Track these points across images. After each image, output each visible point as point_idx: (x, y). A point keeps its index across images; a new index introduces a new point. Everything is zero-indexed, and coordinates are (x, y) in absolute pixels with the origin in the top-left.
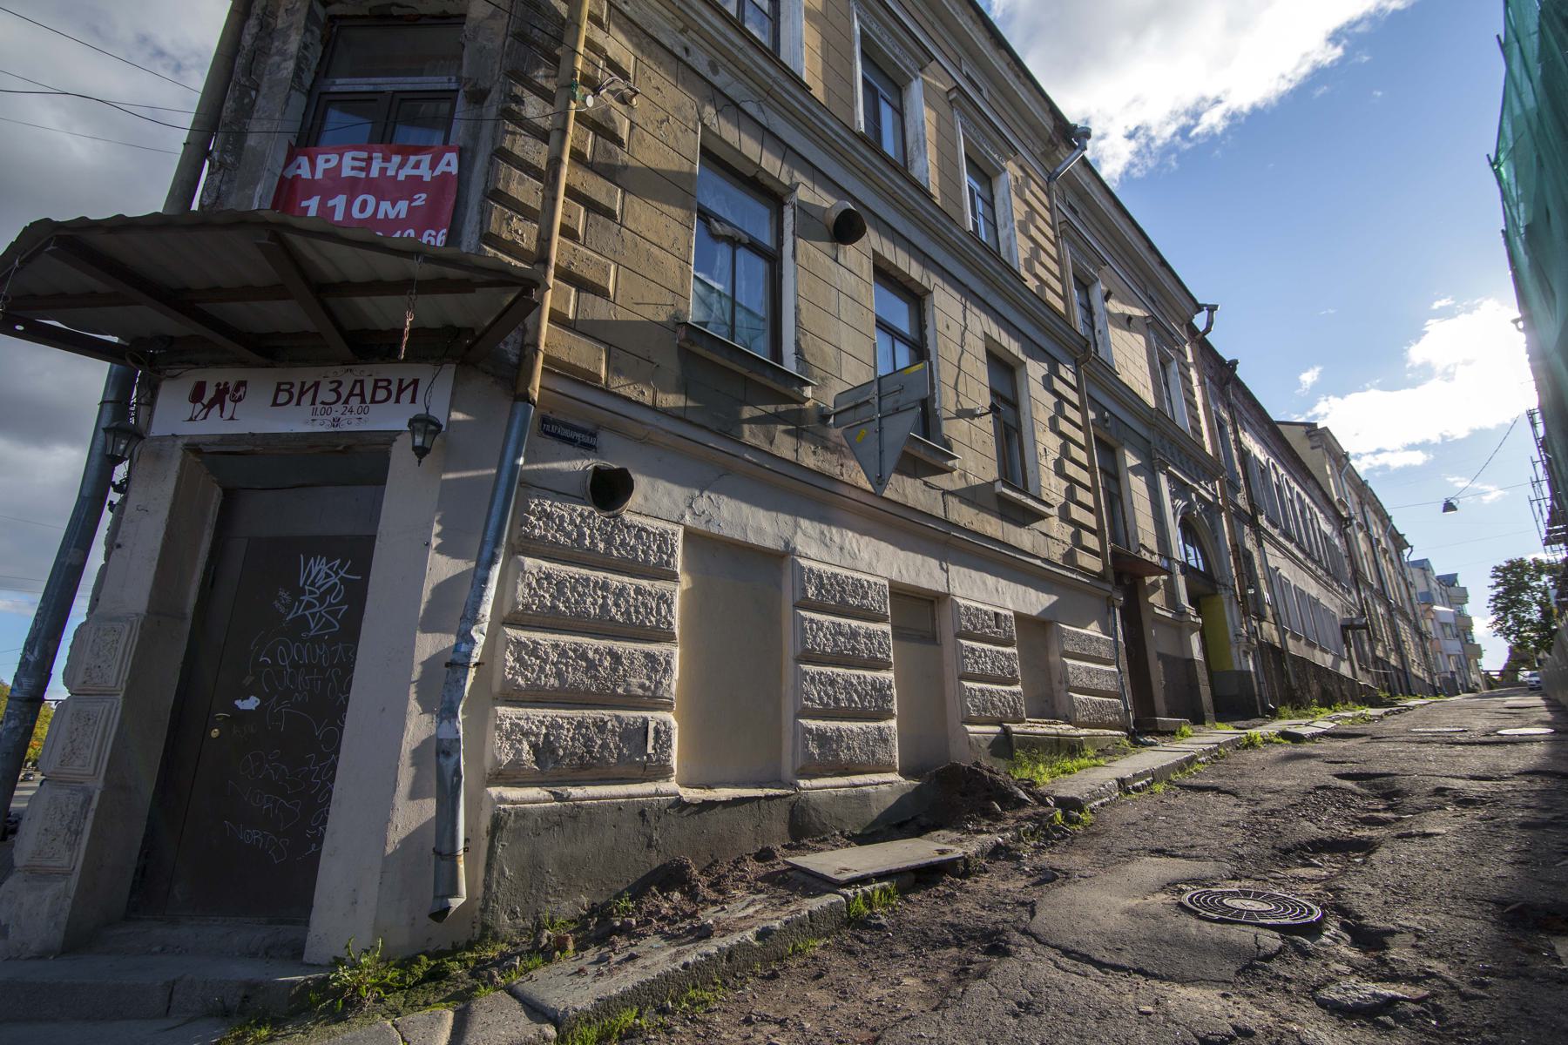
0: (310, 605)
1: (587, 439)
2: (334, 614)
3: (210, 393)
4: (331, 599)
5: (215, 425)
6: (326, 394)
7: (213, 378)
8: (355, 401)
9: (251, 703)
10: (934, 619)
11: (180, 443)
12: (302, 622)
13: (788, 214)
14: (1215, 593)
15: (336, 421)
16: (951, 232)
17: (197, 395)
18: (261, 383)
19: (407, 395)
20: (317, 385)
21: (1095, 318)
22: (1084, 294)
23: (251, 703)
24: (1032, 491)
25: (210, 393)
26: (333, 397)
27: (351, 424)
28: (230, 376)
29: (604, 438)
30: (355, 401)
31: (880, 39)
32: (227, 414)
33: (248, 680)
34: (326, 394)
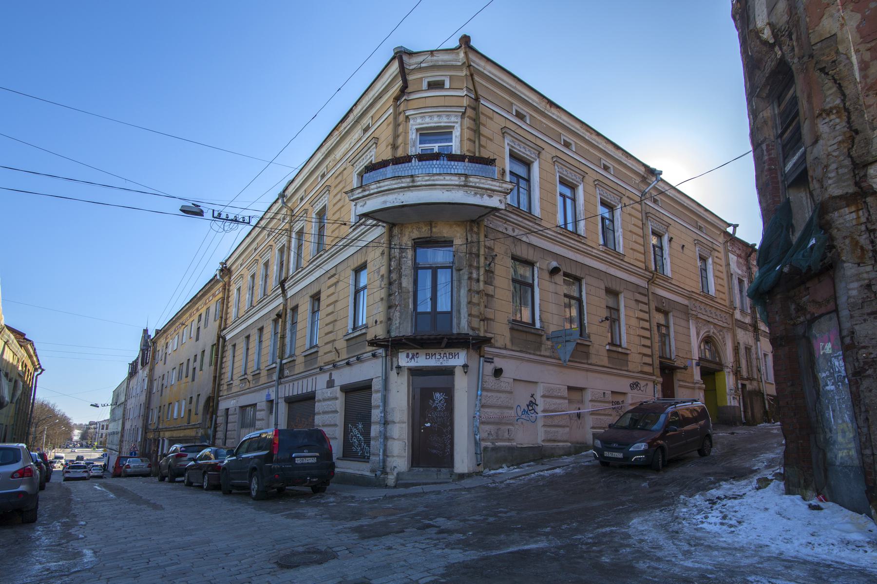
0: (437, 404)
1: (490, 360)
2: (443, 405)
3: (410, 356)
4: (442, 402)
5: (413, 364)
6: (437, 356)
7: (411, 352)
8: (445, 358)
9: (428, 425)
10: (582, 396)
11: (406, 368)
12: (436, 408)
13: (536, 269)
14: (722, 370)
15: (441, 363)
16: (592, 252)
17: (408, 356)
18: (422, 353)
19: (457, 357)
20: (435, 354)
21: (664, 252)
22: (659, 239)
23: (428, 425)
24: (665, 274)
25: (410, 356)
26: (439, 357)
27: (445, 364)
28: (415, 351)
29: (496, 359)
30: (445, 358)
31: (566, 176)
32: (416, 361)
33: (427, 420)
34: (437, 356)
